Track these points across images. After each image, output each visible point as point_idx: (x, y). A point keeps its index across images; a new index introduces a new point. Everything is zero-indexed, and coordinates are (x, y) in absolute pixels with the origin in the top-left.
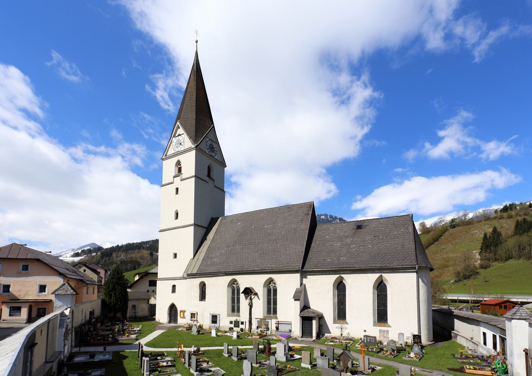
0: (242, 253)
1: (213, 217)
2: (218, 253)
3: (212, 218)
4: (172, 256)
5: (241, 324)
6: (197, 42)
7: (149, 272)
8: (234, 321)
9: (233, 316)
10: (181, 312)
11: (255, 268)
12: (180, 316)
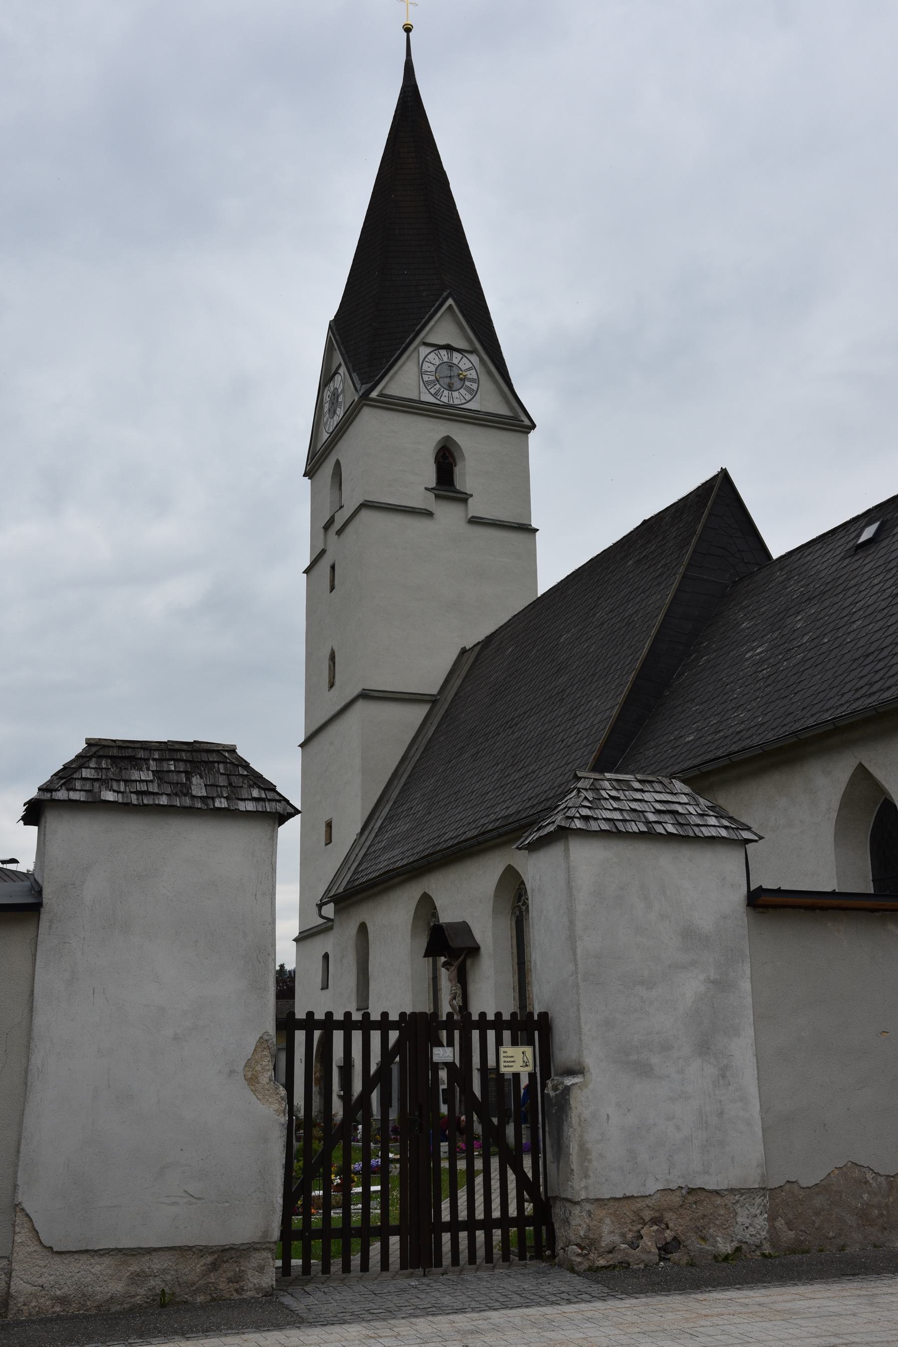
6: (408, 30)
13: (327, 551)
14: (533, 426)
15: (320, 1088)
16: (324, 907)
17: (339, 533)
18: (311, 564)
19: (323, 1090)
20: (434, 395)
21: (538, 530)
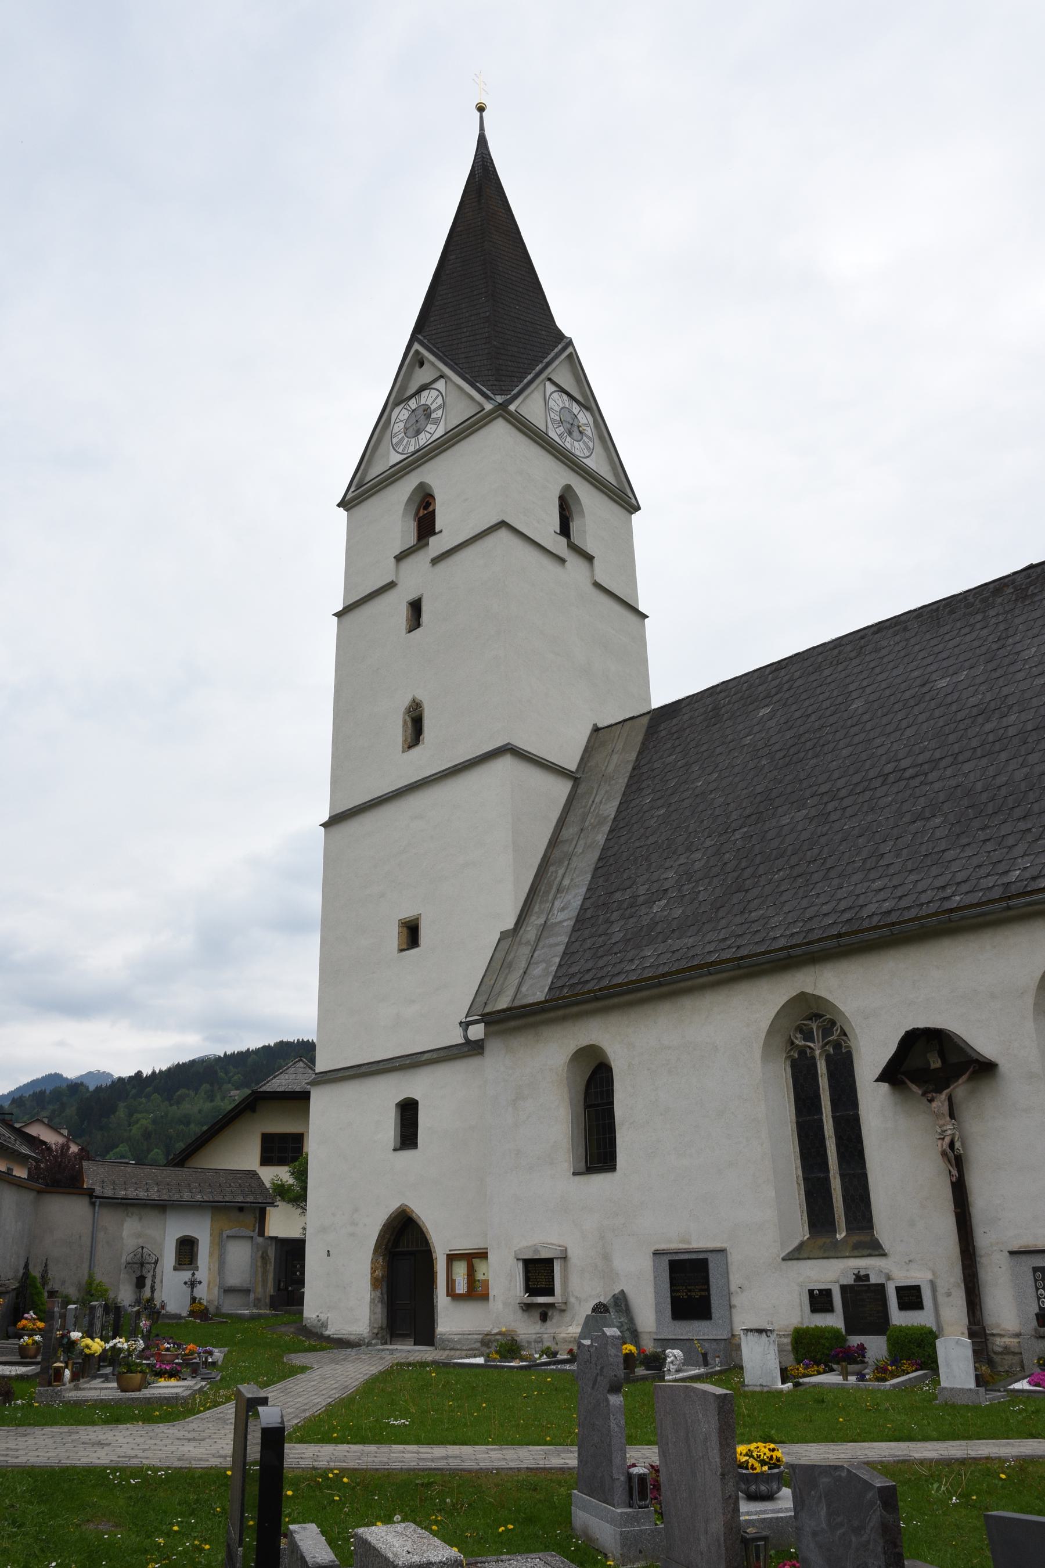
0: (823, 840)
1: (600, 725)
2: (671, 874)
3: (596, 730)
4: (393, 936)
5: (903, 1306)
6: (481, 109)
7: (261, 1090)
8: (844, 1288)
9: (833, 1251)
10: (451, 1258)
11: (948, 898)
12: (451, 1293)
13: (399, 586)
14: (637, 508)
15: (382, 1293)
16: (471, 1027)
17: (435, 561)
18: (344, 608)
19: (385, 1296)
20: (560, 436)
21: (648, 617)
